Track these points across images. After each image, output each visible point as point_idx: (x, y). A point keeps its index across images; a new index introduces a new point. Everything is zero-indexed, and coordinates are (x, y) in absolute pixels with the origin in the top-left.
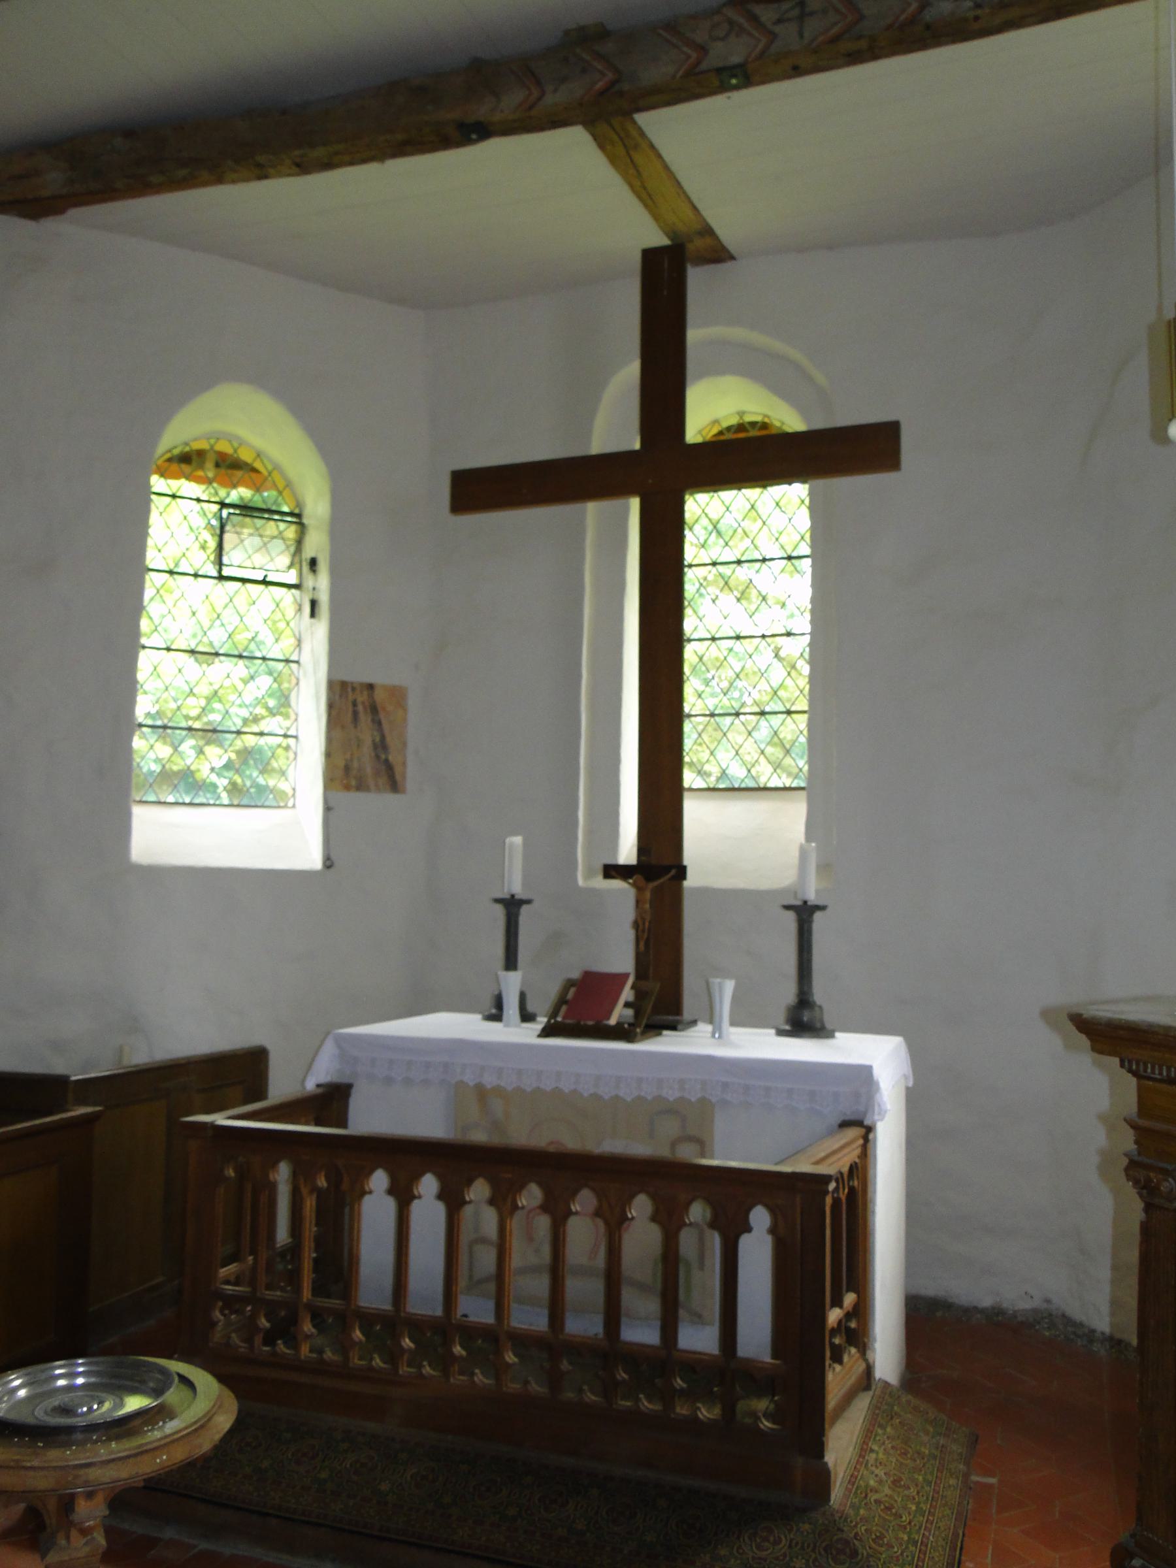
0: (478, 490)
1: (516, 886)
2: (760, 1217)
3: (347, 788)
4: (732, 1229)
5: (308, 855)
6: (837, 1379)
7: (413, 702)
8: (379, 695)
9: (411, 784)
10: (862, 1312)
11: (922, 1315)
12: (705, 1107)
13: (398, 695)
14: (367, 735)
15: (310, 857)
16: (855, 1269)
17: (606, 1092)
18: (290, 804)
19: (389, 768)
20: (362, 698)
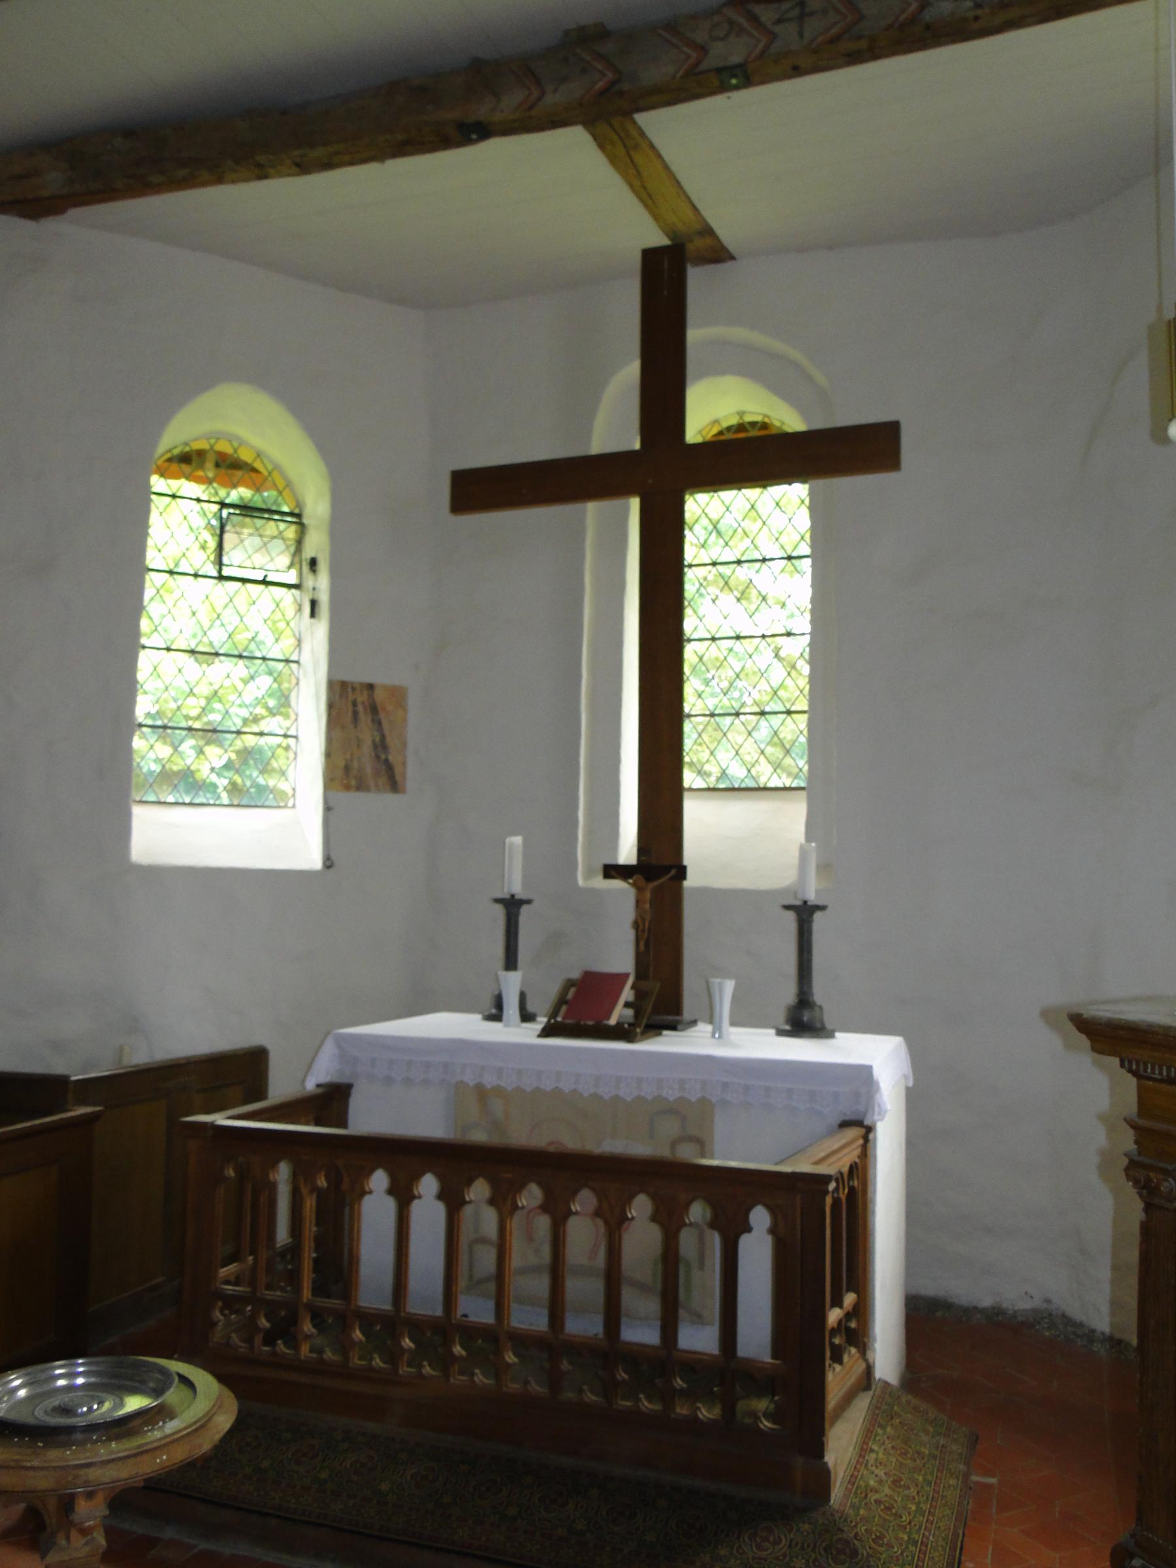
0: (478, 490)
1: (516, 886)
2: (760, 1217)
3: (347, 788)
4: (732, 1229)
5: (308, 855)
6: (837, 1379)
7: (413, 702)
8: (379, 696)
9: (410, 784)
10: (862, 1312)
11: (922, 1315)
12: (705, 1108)
13: (398, 694)
14: (367, 735)
15: (310, 857)
16: (855, 1269)
17: (606, 1092)
18: (290, 804)
19: (389, 768)
20: (362, 698)
